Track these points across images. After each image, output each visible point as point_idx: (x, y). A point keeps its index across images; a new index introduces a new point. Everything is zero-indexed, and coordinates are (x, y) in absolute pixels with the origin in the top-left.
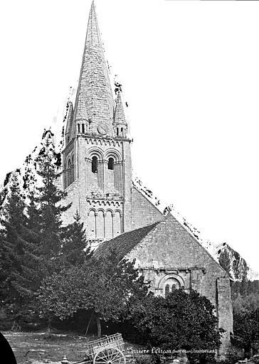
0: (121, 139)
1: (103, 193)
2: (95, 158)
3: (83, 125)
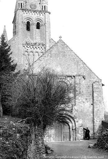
0: (44, 10)
1: (33, 42)
2: (28, 23)
3: (21, 4)
